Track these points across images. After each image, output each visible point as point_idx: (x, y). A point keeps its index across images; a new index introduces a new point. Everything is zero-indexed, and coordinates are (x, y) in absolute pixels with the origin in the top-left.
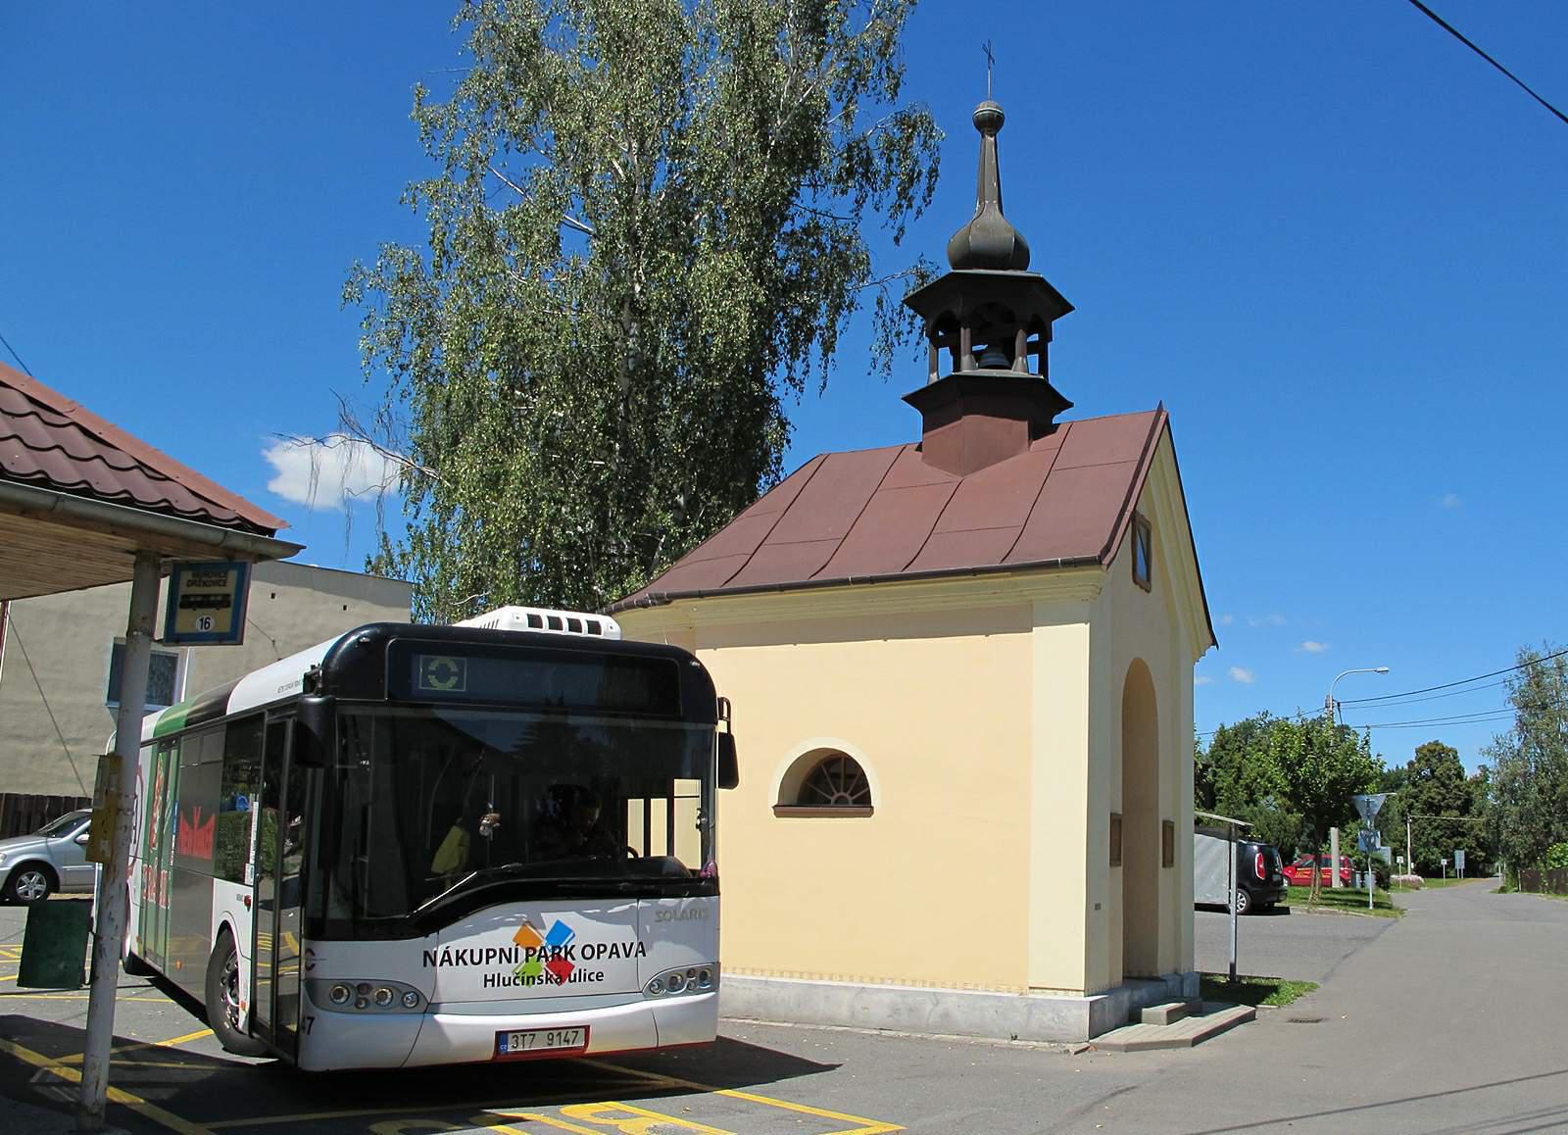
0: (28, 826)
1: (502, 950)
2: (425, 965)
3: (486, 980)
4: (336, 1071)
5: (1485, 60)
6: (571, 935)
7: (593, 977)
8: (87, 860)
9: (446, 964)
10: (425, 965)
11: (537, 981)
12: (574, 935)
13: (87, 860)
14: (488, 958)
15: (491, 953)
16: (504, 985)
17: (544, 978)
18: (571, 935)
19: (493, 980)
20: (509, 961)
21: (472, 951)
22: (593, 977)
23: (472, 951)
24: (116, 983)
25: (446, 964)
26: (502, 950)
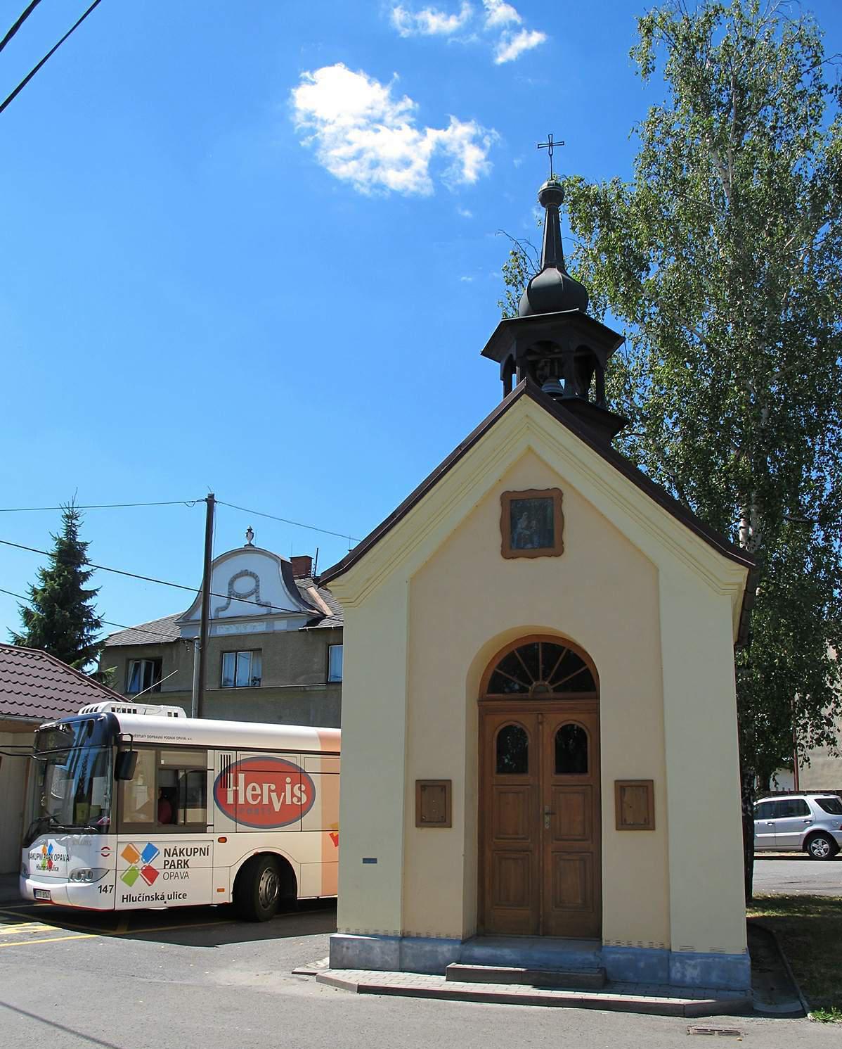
0: (754, 969)
1: (201, 849)
2: (165, 856)
3: (123, 898)
4: (479, 727)
5: (32, 1012)
6: (150, 883)
7: (181, 896)
8: (584, 770)
9: (175, 855)
10: (165, 856)
11: (151, 899)
12: (150, 885)
13: (584, 770)
14: (194, 853)
15: (196, 850)
16: (133, 901)
17: (154, 897)
18: (150, 883)
19: (127, 898)
20: (204, 855)
21: (187, 849)
22: (181, 896)
23: (187, 849)
24: (341, 762)
25: (175, 855)
26: (201, 849)
